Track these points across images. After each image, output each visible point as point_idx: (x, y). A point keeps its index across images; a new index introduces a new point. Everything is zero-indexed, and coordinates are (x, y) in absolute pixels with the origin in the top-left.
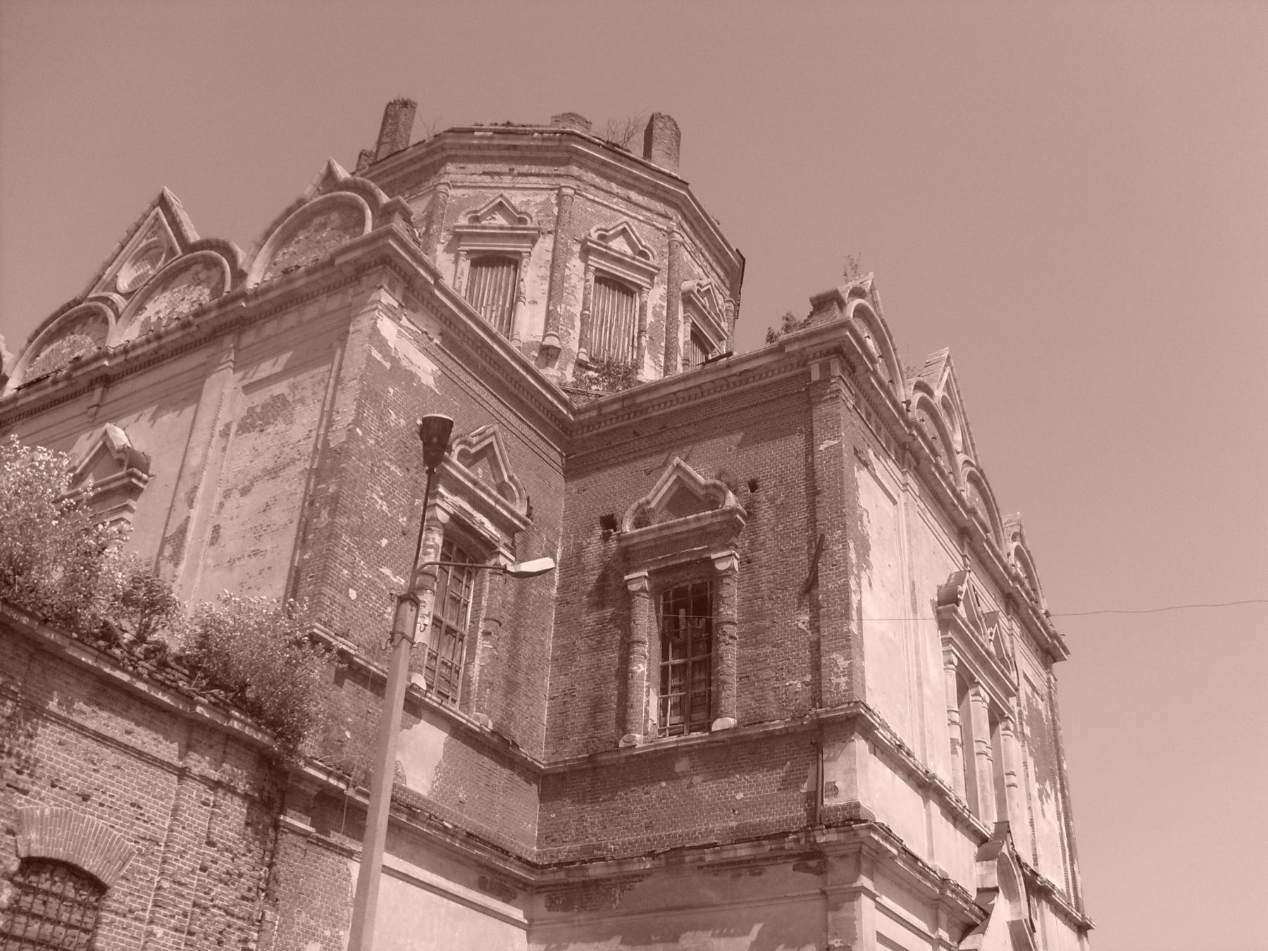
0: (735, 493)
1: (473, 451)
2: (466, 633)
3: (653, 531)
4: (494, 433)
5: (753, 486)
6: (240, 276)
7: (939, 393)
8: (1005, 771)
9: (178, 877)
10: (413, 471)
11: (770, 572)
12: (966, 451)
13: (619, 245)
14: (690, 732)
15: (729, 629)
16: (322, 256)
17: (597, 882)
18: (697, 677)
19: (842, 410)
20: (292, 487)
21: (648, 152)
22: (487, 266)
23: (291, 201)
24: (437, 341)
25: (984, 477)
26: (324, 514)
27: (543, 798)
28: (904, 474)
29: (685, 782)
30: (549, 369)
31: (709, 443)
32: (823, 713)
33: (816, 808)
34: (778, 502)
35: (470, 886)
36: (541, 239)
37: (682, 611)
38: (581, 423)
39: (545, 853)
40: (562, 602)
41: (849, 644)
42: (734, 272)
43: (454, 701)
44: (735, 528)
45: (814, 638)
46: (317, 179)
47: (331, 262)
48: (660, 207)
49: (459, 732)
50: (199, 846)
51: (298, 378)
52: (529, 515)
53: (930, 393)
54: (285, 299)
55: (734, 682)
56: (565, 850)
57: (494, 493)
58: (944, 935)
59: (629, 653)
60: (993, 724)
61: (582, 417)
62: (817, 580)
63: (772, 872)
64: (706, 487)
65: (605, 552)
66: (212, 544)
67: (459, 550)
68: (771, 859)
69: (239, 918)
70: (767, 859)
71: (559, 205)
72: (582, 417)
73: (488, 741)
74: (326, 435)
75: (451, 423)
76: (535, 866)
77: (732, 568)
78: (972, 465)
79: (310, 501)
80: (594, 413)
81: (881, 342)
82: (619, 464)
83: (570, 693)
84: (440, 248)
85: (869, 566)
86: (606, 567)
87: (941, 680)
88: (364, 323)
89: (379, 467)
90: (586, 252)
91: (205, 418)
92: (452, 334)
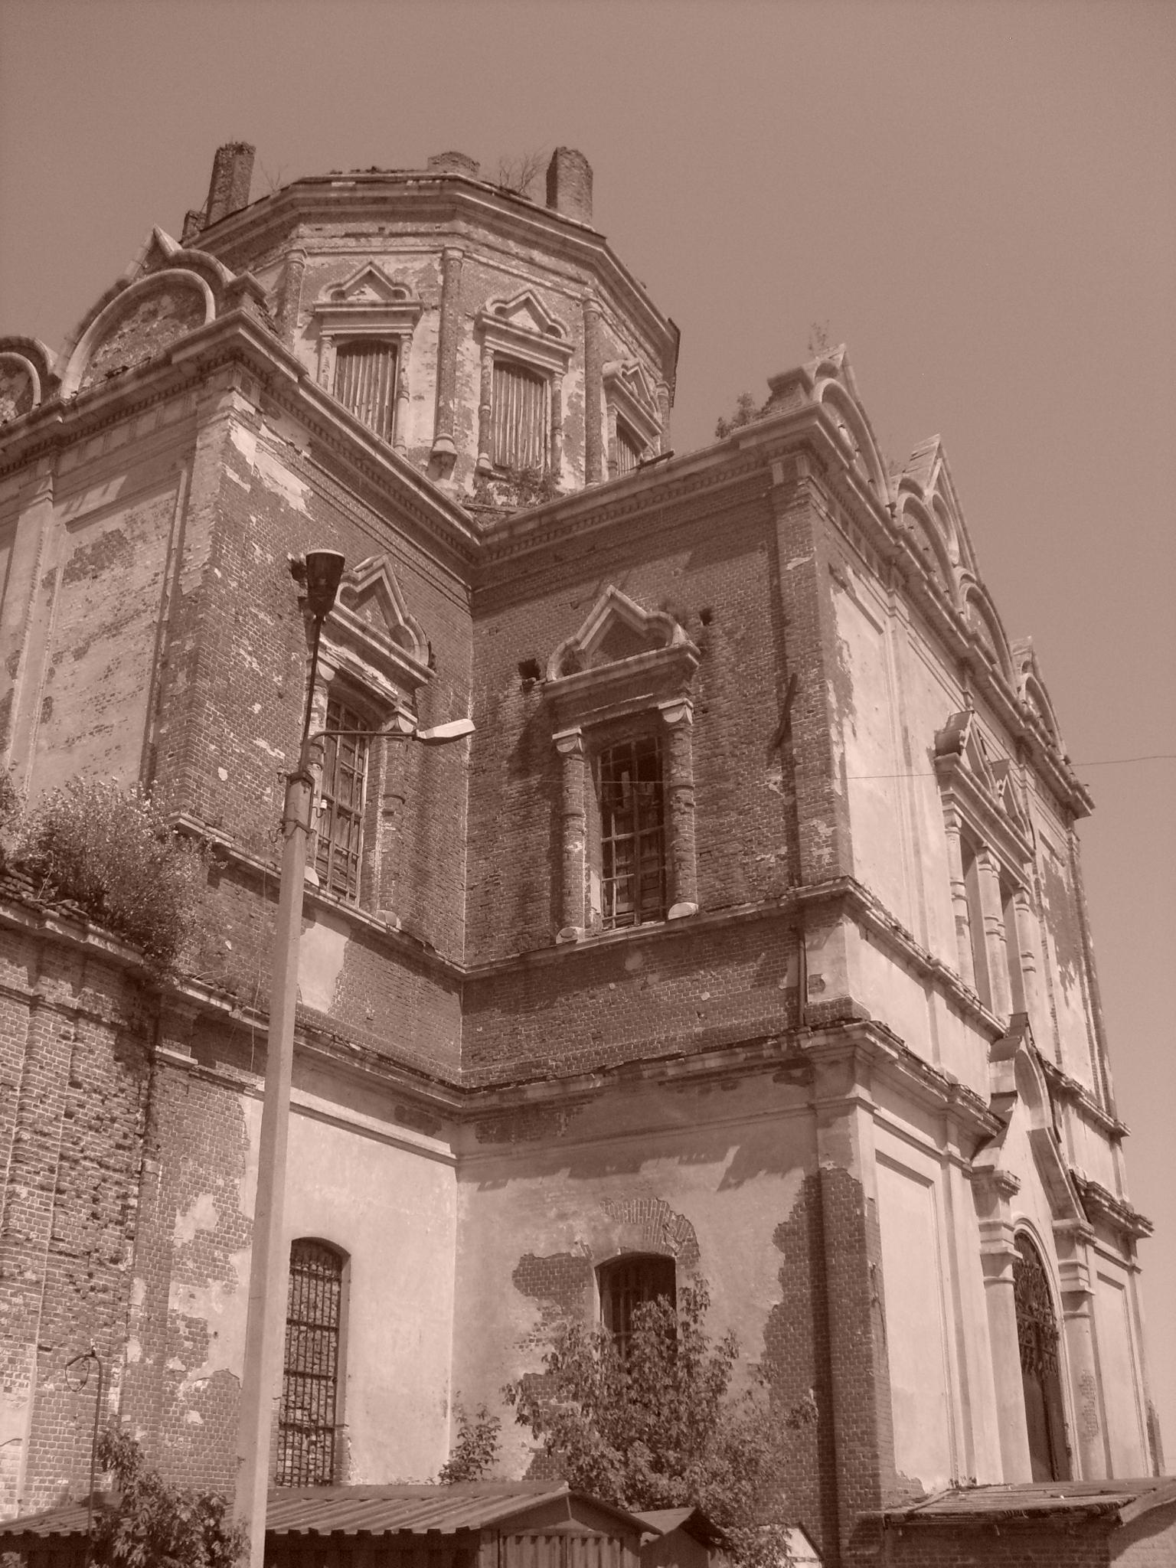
0: (684, 627)
1: (359, 589)
2: (362, 812)
3: (585, 678)
4: (383, 566)
5: (706, 617)
6: (52, 383)
7: (929, 492)
8: (1020, 952)
9: (39, 1127)
10: (287, 618)
11: (731, 722)
12: (963, 563)
13: (522, 320)
14: (643, 920)
15: (685, 795)
16: (155, 352)
17: (537, 1107)
18: (647, 855)
19: (814, 521)
20: (138, 645)
21: (552, 200)
22: (358, 354)
23: (110, 284)
24: (306, 454)
25: (987, 594)
26: (182, 677)
27: (465, 1009)
28: (890, 595)
29: (638, 982)
30: (444, 481)
31: (649, 566)
32: (804, 892)
33: (798, 1007)
34: (738, 636)
35: (385, 1118)
36: (424, 317)
37: (625, 775)
38: (488, 547)
39: (472, 1075)
40: (476, 771)
41: (832, 807)
42: (666, 348)
43: (353, 897)
44: (687, 670)
45: (789, 801)
46: (140, 253)
47: (167, 361)
48: (571, 269)
49: (363, 935)
50: (63, 1089)
51: (136, 509)
52: (431, 665)
53: (919, 492)
54: (110, 410)
55: (693, 859)
56: (497, 1069)
57: (388, 640)
58: (955, 1150)
59: (562, 830)
60: (1006, 897)
61: (489, 541)
62: (790, 735)
63: (748, 1085)
64: (648, 621)
65: (526, 706)
66: (44, 721)
67: (348, 713)
68: (747, 1069)
69: (115, 1170)
70: (741, 1070)
71: (444, 271)
72: (489, 541)
73: (398, 943)
74: (176, 579)
75: (342, 560)
76: (462, 1090)
77: (684, 720)
78: (972, 581)
79: (163, 662)
80: (504, 535)
81: (857, 430)
82: (539, 596)
83: (492, 881)
84: (297, 333)
85: (852, 711)
86: (529, 725)
87: (942, 846)
88: (213, 435)
89: (245, 616)
90: (481, 331)
91: (22, 566)
92: (324, 444)
